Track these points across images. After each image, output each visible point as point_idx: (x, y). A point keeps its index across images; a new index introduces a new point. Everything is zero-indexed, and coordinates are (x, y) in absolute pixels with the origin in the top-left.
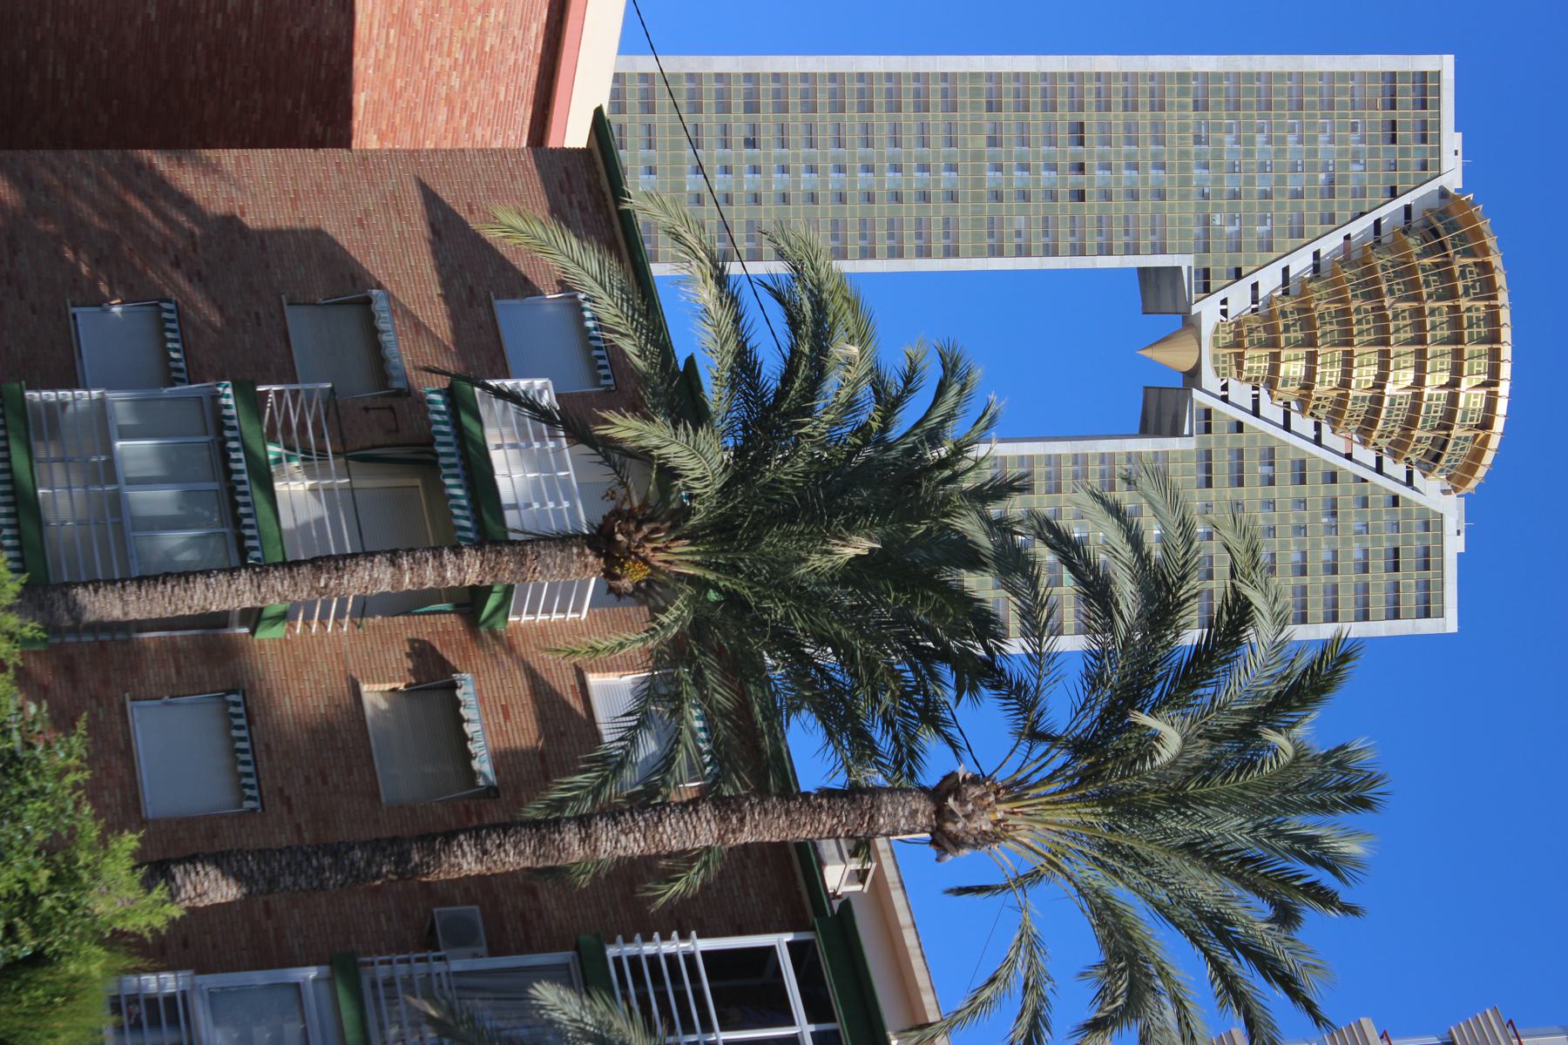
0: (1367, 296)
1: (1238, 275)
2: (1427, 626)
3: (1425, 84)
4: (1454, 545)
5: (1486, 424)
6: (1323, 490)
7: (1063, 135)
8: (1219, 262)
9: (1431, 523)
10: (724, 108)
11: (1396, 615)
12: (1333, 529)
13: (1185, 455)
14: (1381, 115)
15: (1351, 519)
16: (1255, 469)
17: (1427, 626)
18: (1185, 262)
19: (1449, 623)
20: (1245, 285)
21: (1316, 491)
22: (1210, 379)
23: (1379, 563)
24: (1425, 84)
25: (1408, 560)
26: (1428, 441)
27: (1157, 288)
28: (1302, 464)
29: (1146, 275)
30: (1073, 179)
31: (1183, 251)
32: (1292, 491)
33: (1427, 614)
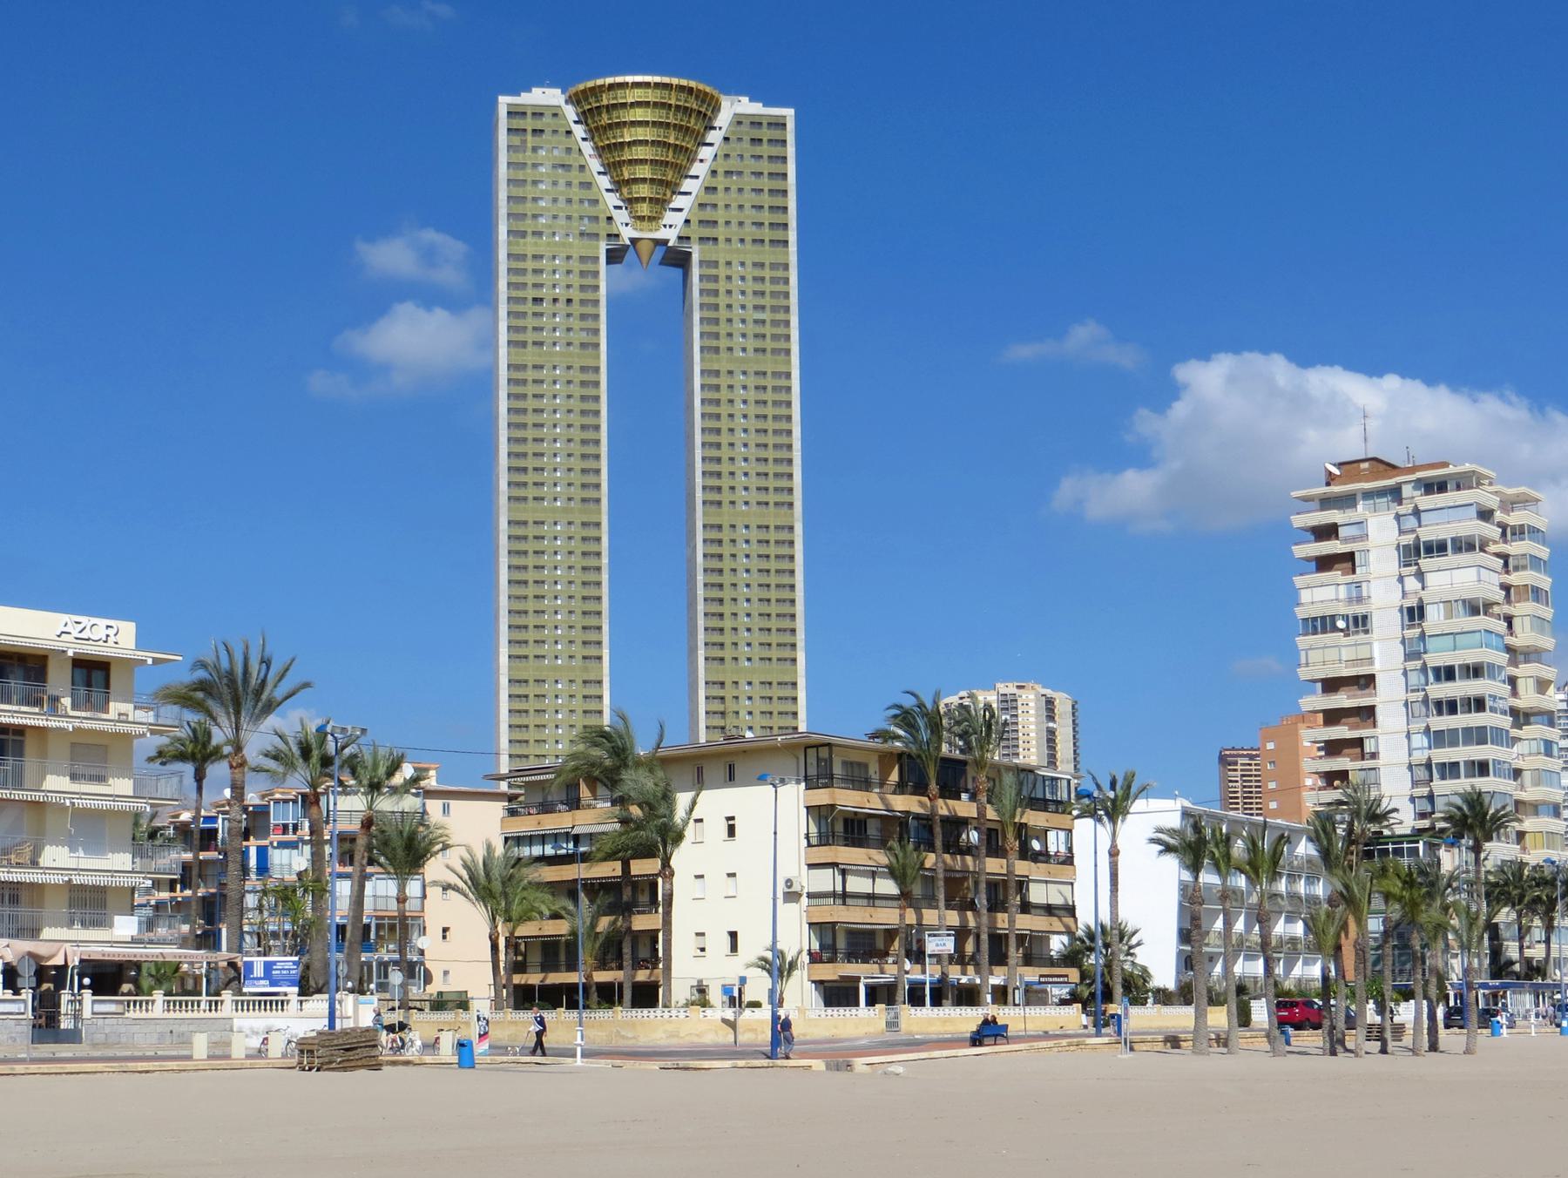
0: (600, 114)
1: (610, 219)
2: (791, 125)
3: (780, 124)
4: (756, 108)
5: (690, 90)
6: (720, 177)
7: (538, 309)
8: (603, 228)
9: (738, 121)
10: (524, 426)
11: (784, 142)
12: (740, 173)
13: (701, 252)
14: (529, 137)
15: (733, 164)
16: (708, 214)
17: (791, 125)
18: (603, 247)
19: (789, 113)
20: (615, 214)
21: (721, 182)
22: (661, 234)
23: (758, 150)
24: (780, 124)
25: (756, 133)
26: (694, 116)
27: (614, 256)
28: (707, 189)
29: (609, 262)
30: (563, 299)
31: (597, 248)
32: (721, 194)
33: (784, 125)
